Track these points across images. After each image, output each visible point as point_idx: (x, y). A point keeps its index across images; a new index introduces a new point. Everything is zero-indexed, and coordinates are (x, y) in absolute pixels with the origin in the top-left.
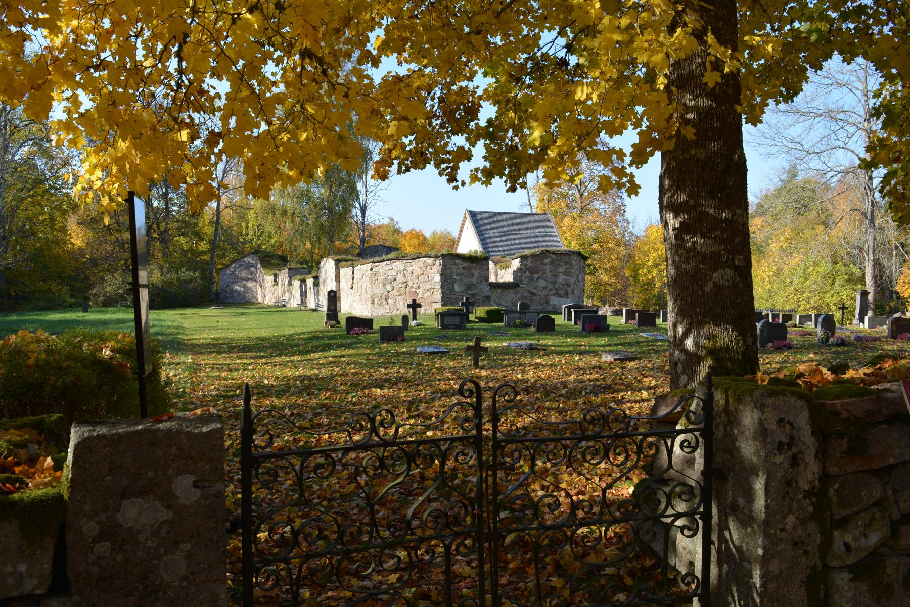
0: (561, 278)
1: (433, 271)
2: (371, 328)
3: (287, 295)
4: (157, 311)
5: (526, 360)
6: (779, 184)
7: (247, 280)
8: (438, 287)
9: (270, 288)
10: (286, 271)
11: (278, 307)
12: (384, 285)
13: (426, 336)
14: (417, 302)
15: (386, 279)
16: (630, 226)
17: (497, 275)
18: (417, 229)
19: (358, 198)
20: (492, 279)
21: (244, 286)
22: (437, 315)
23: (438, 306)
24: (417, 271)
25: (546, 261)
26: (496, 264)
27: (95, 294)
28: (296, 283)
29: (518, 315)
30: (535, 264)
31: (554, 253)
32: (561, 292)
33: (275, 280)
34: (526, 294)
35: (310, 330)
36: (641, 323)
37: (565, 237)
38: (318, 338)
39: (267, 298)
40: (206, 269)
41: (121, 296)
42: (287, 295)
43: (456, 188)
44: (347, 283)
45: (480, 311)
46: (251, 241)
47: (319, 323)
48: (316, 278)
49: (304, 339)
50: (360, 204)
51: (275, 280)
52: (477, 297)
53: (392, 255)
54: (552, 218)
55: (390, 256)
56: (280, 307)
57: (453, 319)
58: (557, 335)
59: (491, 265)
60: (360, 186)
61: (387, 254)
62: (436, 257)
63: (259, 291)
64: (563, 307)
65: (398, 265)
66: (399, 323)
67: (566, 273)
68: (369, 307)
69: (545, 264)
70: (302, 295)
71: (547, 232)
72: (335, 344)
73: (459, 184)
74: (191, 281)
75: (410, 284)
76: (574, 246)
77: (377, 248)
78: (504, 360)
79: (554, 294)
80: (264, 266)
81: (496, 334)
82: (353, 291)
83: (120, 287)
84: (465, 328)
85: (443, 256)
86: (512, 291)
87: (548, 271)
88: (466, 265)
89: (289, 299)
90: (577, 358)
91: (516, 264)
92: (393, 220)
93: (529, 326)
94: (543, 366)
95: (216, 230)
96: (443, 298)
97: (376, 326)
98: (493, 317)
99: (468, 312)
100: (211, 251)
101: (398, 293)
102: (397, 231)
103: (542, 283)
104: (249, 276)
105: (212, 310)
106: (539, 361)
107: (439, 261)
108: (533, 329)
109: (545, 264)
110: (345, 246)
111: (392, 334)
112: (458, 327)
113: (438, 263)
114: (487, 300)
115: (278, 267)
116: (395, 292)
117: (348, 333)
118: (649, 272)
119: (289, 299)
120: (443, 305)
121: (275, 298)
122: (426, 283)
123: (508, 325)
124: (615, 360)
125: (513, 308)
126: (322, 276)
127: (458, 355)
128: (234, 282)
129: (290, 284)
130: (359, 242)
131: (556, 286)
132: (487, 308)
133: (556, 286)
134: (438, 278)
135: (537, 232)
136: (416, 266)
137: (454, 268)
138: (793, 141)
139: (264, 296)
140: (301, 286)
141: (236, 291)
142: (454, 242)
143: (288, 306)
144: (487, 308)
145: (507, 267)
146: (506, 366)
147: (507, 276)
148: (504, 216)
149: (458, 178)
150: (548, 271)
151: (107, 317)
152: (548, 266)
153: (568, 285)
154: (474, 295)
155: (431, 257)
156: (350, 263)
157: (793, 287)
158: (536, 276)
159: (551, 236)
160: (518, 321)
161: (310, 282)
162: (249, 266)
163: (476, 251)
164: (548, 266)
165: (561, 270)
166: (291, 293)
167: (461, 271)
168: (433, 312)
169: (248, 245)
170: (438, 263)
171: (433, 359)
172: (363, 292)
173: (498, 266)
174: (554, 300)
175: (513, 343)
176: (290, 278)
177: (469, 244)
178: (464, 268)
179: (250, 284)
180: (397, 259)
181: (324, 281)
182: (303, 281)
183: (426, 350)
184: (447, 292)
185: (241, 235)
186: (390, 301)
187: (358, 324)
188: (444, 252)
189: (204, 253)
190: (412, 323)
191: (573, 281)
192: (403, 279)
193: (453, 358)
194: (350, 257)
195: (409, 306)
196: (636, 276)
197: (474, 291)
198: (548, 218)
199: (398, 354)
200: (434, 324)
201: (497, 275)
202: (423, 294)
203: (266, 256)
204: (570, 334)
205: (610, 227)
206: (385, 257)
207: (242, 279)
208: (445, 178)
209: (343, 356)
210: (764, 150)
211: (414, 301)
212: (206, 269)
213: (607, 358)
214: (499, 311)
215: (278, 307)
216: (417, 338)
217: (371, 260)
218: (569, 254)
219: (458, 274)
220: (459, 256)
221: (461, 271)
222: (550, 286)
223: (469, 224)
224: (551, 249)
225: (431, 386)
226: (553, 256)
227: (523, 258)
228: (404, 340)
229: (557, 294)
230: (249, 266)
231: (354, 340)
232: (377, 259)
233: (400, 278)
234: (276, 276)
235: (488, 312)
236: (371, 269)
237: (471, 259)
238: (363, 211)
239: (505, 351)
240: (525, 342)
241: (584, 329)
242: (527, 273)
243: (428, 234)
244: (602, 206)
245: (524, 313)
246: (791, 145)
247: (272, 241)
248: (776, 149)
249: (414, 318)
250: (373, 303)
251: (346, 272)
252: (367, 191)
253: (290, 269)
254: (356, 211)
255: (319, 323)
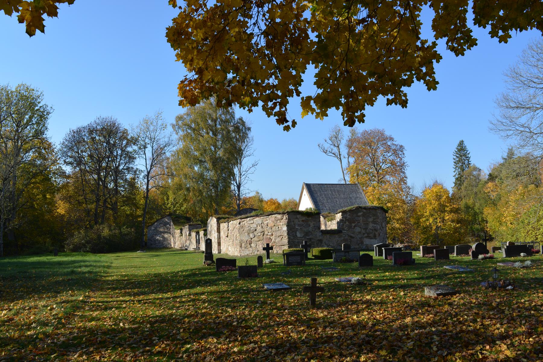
0: (371, 226)
1: (281, 224)
2: (235, 266)
3: (188, 242)
4: (99, 255)
5: (357, 297)
6: (502, 161)
7: (165, 232)
8: (286, 234)
9: (179, 238)
10: (187, 226)
11: (182, 250)
12: (249, 234)
13: (276, 274)
14: (270, 245)
15: (249, 230)
16: (411, 190)
17: (326, 225)
18: (274, 198)
19: (235, 179)
20: (323, 228)
21: (163, 237)
22: (284, 255)
23: (286, 247)
24: (271, 224)
25: (360, 214)
26: (325, 218)
27: (68, 244)
28: (194, 234)
29: (343, 254)
30: (352, 217)
31: (365, 208)
32: (371, 235)
33: (181, 233)
34: (347, 237)
35: (190, 267)
36: (438, 257)
37: (369, 198)
38: (194, 275)
39: (177, 244)
40: (139, 227)
41: (84, 245)
42: (188, 242)
43: (287, 128)
44: (224, 233)
45: (315, 251)
46: (170, 208)
47: (200, 262)
48: (205, 231)
49: (184, 276)
50: (236, 183)
51: (181, 233)
52: (313, 241)
53: (253, 213)
54: (360, 187)
55: (252, 214)
56: (184, 250)
57: (295, 258)
58: (376, 269)
59: (322, 219)
60: (236, 170)
61: (250, 213)
62: (284, 213)
63: (172, 240)
64: (375, 246)
65: (258, 220)
66: (255, 263)
67: (374, 222)
68: (238, 250)
69: (359, 216)
70: (197, 242)
71: (358, 195)
72: (205, 280)
73: (290, 124)
74: (128, 234)
75: (266, 233)
76: (376, 204)
77: (246, 209)
78: (338, 296)
79: (366, 237)
80: (175, 224)
81: (328, 271)
82: (228, 239)
83: (83, 239)
84: (305, 265)
85: (288, 213)
86: (337, 236)
87: (361, 221)
88: (304, 218)
89: (189, 245)
90: (402, 293)
91: (339, 216)
92: (258, 193)
93: (352, 261)
94: (375, 303)
95: (146, 201)
96: (289, 242)
97: (238, 264)
98: (324, 255)
99: (307, 252)
100: (143, 216)
101: (258, 240)
102: (261, 201)
103: (358, 229)
104: (166, 230)
105: (139, 253)
106: (368, 297)
107: (286, 217)
108: (356, 264)
109: (359, 216)
110: (228, 209)
111: (249, 272)
112: (300, 264)
113: (285, 218)
114: (319, 243)
115: (183, 224)
116: (256, 239)
117: (217, 271)
118: (427, 220)
119: (189, 245)
120: (289, 247)
121: (181, 244)
122: (276, 233)
123: (336, 261)
124: (439, 295)
125: (339, 248)
126: (209, 229)
127: (298, 292)
128: (156, 235)
129: (190, 235)
130: (237, 208)
131: (367, 231)
132: (320, 249)
133: (367, 231)
134: (285, 228)
135: (351, 196)
136: (270, 221)
137: (296, 221)
138: (523, 126)
139: (175, 243)
140: (196, 236)
141: (158, 240)
142: (298, 204)
143: (189, 249)
144: (320, 249)
145: (332, 220)
146: (340, 305)
147: (333, 225)
148: (328, 186)
149: (288, 117)
150: (361, 221)
151: (73, 259)
152: (361, 218)
153: (376, 230)
154: (310, 239)
155: (280, 214)
156: (226, 220)
157: (530, 226)
158: (353, 225)
159: (360, 198)
160: (343, 258)
161: (202, 233)
162: (165, 224)
163: (311, 209)
164: (361, 218)
165: (371, 220)
166: (190, 240)
167: (301, 223)
168: (282, 252)
169: (168, 210)
170: (285, 218)
171: (276, 296)
172: (231, 240)
173: (326, 219)
174: (367, 241)
175: (343, 278)
176: (190, 231)
177: (306, 204)
178: (303, 221)
179: (166, 236)
180: (257, 216)
181: (210, 232)
182: (198, 233)
183: (272, 287)
184: (292, 238)
185: (164, 204)
186: (252, 245)
187: (227, 263)
188: (289, 210)
189: (139, 216)
190: (266, 261)
191: (379, 228)
192: (261, 230)
193: (294, 295)
194: (227, 216)
195: (264, 249)
196: (418, 223)
197: (311, 237)
198: (358, 187)
199: (248, 291)
200: (281, 261)
201: (326, 225)
202: (275, 239)
203: (176, 217)
204: (386, 268)
205: (398, 192)
206: (249, 215)
207: (161, 232)
208: (273, 119)
209: (203, 293)
210: (503, 134)
211: (268, 245)
212: (139, 227)
213: (429, 293)
214: (329, 250)
215: (182, 250)
216: (267, 275)
217: (240, 217)
218: (375, 208)
219: (299, 225)
220: (302, 213)
221: (301, 223)
222: (363, 231)
223: (305, 192)
224: (362, 205)
225: (268, 334)
226: (365, 211)
227: (344, 213)
228: (257, 276)
229: (368, 237)
230: (165, 224)
231: (220, 277)
232: (243, 216)
233: (259, 229)
234: (181, 230)
235: (321, 252)
236: (239, 223)
237: (307, 214)
238: (239, 187)
239: (336, 287)
240: (355, 278)
241: (395, 263)
242: (347, 223)
243: (280, 201)
244: (391, 179)
245: (348, 252)
246: (522, 129)
247: (183, 208)
248: (511, 132)
249: (268, 257)
250: (241, 247)
251: (223, 226)
252: (241, 175)
253: (190, 225)
254: (233, 187)
255: (200, 262)
